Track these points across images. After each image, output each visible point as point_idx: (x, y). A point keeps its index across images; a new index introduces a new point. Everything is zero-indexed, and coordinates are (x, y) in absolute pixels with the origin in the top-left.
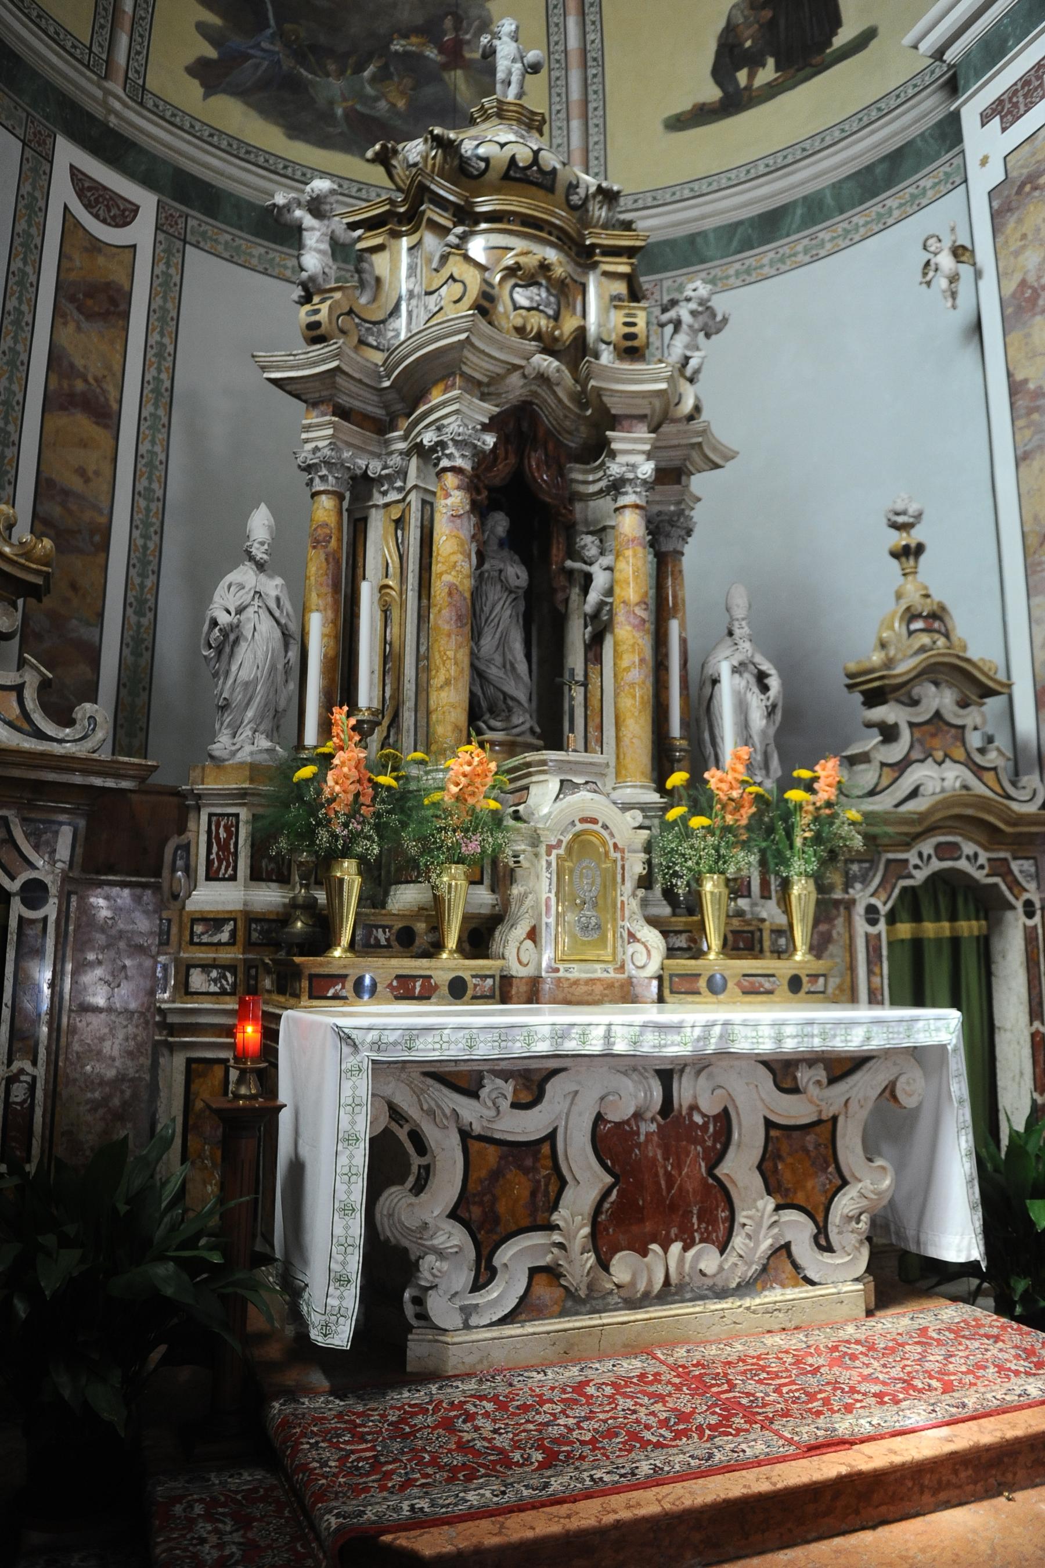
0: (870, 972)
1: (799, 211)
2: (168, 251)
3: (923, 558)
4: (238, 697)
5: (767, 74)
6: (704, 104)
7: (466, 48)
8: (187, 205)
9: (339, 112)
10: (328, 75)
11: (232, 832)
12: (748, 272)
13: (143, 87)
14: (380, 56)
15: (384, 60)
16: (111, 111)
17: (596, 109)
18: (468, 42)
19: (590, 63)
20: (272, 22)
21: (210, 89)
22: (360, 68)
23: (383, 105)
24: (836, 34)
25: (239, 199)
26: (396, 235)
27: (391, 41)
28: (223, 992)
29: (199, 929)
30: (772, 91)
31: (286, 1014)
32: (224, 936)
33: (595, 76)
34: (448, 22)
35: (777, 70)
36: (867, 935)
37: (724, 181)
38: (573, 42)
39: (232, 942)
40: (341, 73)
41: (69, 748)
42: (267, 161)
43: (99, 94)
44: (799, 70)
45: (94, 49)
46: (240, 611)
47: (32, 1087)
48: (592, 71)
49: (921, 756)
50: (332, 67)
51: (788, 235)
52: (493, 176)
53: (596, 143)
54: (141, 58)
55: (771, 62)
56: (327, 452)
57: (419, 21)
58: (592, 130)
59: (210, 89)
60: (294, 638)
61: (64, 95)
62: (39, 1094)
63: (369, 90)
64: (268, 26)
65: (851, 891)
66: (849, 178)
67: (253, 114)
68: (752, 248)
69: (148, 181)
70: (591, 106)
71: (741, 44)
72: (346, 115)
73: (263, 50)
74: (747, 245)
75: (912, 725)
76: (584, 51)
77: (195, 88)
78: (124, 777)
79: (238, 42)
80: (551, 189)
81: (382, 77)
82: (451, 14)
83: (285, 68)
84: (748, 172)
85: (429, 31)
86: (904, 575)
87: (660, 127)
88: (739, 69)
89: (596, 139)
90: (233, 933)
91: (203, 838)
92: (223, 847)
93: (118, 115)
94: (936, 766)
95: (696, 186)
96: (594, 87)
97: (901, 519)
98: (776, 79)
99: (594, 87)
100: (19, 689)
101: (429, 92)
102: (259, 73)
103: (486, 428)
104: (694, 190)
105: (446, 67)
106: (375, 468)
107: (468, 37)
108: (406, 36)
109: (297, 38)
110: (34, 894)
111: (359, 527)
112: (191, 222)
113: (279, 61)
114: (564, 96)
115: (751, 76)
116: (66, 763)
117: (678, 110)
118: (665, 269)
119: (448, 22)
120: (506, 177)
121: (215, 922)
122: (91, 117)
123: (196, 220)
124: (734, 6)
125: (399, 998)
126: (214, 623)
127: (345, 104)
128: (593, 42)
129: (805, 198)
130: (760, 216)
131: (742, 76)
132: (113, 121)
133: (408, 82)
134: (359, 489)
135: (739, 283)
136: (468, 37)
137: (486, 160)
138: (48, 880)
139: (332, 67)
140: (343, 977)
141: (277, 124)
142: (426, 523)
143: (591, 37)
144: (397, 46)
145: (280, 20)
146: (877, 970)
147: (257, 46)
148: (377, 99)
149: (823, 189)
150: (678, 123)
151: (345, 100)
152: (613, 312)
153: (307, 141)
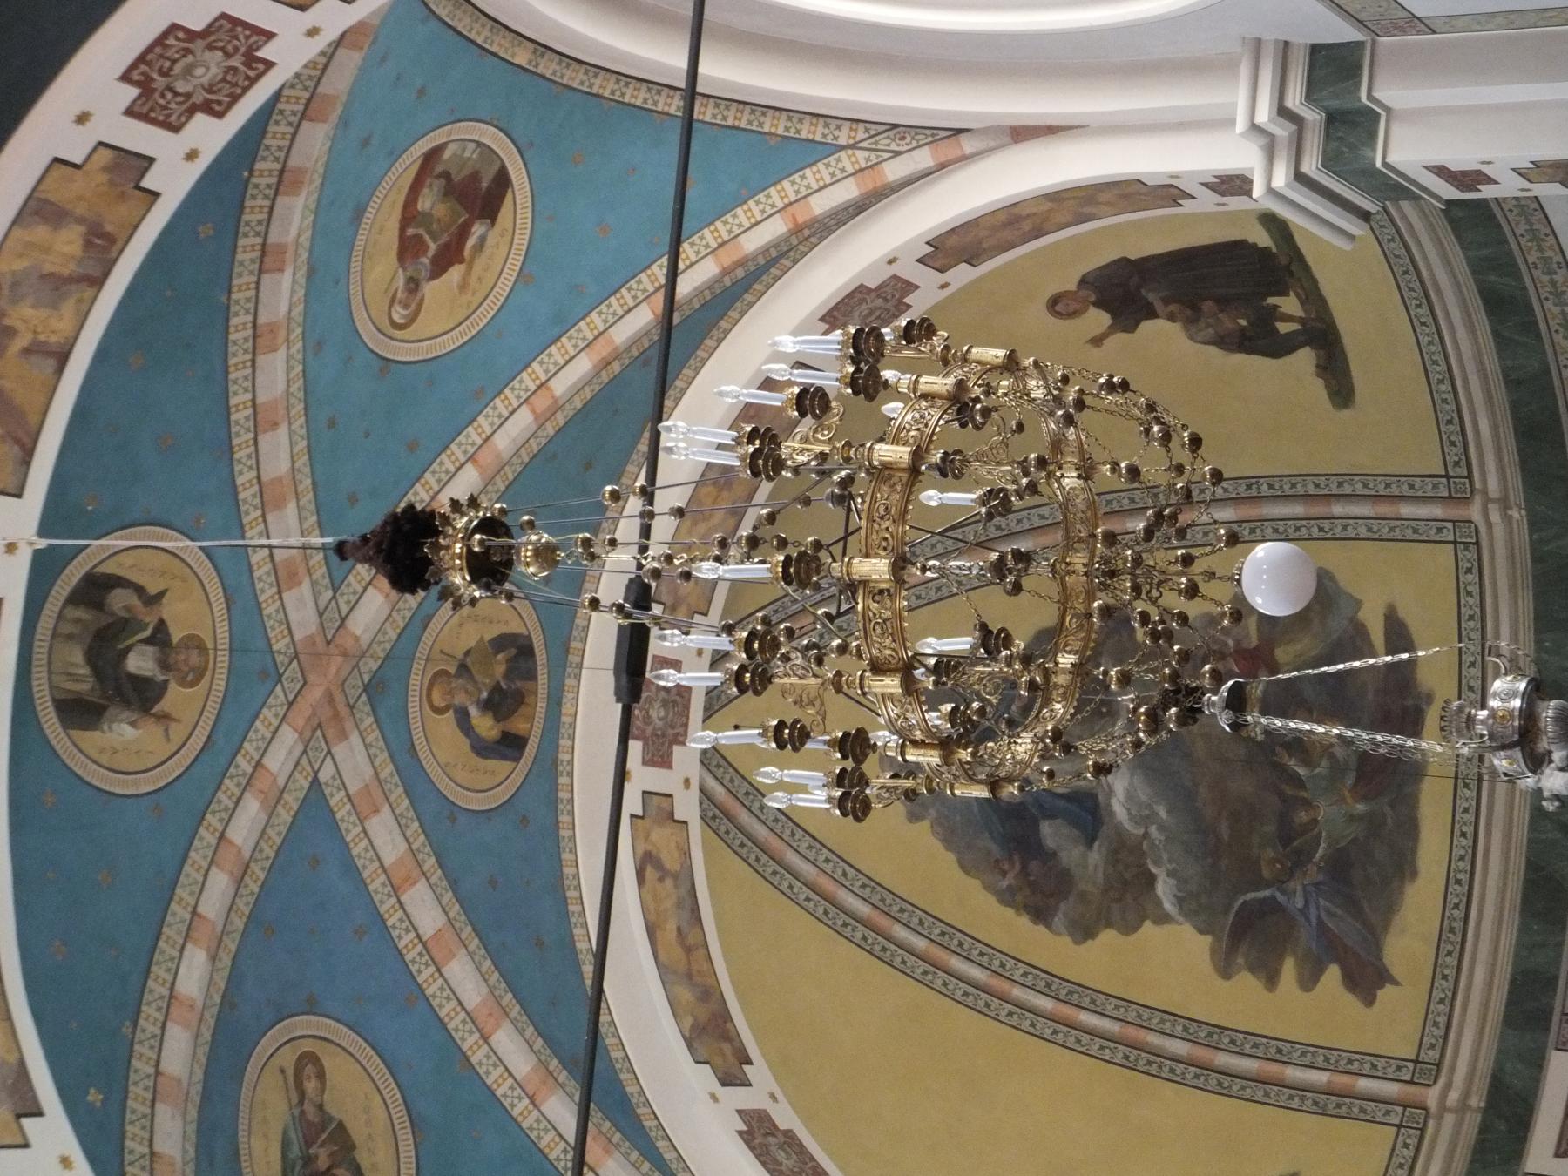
6: (1318, 366)
7: (1245, 645)
8: (1551, 1013)
9: (1361, 808)
10: (1315, 821)
13: (1416, 1062)
14: (1273, 752)
15: (1278, 749)
16: (1463, 1106)
17: (1317, 486)
18: (1238, 642)
19: (1254, 492)
20: (1267, 893)
21: (1383, 977)
24: (1255, 246)
25: (1520, 944)
27: (1253, 740)
30: (1313, 297)
33: (1271, 487)
35: (1284, 293)
37: (1433, 348)
42: (1456, 906)
43: (1449, 1119)
44: (1291, 274)
45: (1397, 1121)
50: (1302, 816)
51: (1525, 289)
53: (1365, 486)
54: (1380, 1063)
55: (1271, 300)
58: (1347, 489)
59: (1383, 977)
61: (1472, 1162)
64: (1273, 898)
67: (1397, 921)
68: (1536, 323)
69: (1537, 1064)
70: (1311, 490)
71: (1243, 329)
72: (1365, 798)
73: (1306, 902)
74: (1530, 326)
77: (1386, 994)
79: (1305, 935)
83: (1321, 877)
87: (1345, 414)
89: (1359, 486)
93: (1466, 1095)
96: (1287, 487)
98: (1298, 296)
99: (1287, 487)
102: (1339, 912)
107: (1231, 643)
109: (1278, 861)
113: (1316, 885)
114: (1299, 523)
115: (1288, 318)
117: (1324, 393)
122: (1484, 1129)
124: (1191, 338)
127: (1349, 800)
129: (1474, 273)
131: (1284, 328)
132: (1478, 1101)
136: (1231, 643)
139: (1302, 816)
141: (1402, 893)
145: (1259, 884)
147: (1304, 911)
149: (1467, 258)
150: (1341, 390)
151: (1343, 800)
152: (1247, 100)
153: (1414, 851)
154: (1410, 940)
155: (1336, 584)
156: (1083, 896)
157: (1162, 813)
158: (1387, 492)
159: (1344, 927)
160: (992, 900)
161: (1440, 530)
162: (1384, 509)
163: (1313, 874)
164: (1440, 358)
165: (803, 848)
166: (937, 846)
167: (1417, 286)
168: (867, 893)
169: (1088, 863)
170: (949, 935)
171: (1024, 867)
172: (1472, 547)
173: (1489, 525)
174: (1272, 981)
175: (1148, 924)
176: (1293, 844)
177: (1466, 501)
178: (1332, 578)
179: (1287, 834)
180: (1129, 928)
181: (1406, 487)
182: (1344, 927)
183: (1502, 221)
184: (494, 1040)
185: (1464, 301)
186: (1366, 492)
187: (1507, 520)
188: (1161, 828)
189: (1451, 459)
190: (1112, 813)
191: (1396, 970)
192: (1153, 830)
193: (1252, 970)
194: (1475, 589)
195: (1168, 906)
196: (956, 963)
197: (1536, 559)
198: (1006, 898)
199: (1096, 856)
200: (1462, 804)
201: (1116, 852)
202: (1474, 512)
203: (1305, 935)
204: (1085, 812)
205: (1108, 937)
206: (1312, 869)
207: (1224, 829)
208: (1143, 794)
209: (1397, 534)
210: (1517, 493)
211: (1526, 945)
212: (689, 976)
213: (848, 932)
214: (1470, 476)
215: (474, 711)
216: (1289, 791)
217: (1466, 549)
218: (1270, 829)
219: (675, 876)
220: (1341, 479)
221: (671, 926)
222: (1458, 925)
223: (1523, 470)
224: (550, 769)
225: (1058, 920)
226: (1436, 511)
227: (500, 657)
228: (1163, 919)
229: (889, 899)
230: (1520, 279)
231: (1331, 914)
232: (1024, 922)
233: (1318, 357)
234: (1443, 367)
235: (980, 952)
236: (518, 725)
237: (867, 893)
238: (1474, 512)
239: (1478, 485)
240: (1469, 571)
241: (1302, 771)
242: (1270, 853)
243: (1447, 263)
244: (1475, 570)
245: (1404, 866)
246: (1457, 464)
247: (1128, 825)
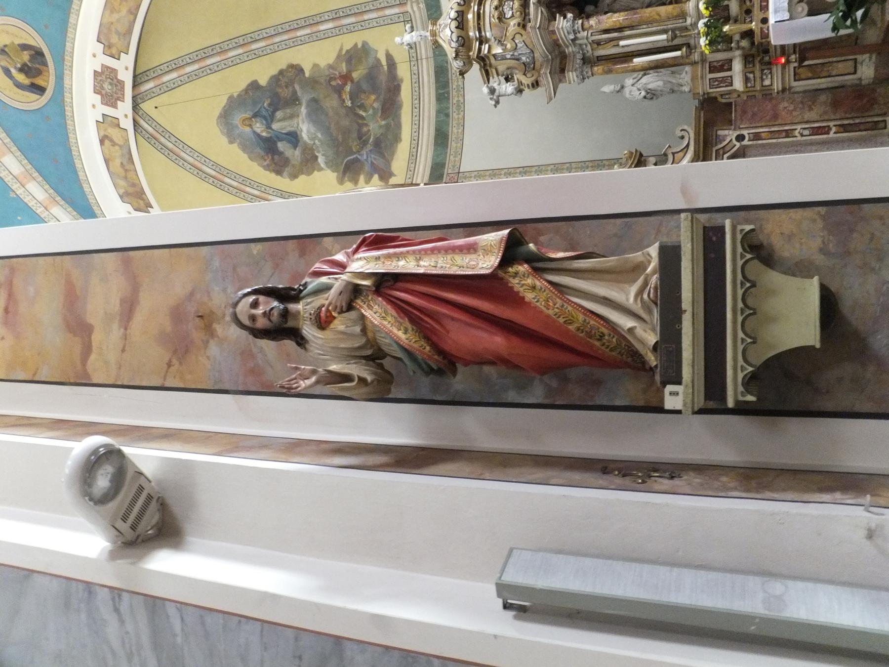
2: (465, 178)
4: (669, 86)
11: (716, 79)
22: (362, 118)
23: (376, 105)
26: (491, 66)
28: (771, 73)
29: (749, 85)
31: (773, 42)
32: (751, 76)
34: (333, 83)
38: (330, 25)
39: (753, 72)
40: (366, 125)
41: (692, 135)
46: (639, 90)
47: (805, 129)
52: (463, 34)
56: (578, 72)
57: (336, 96)
58: (367, 8)
59: (391, 174)
60: (646, 69)
62: (807, 126)
63: (371, 112)
67: (396, 157)
72: (384, 119)
78: (700, 116)
79: (367, 168)
80: (462, 12)
81: (362, 107)
82: (329, 82)
85: (339, 91)
90: (750, 73)
91: (718, 90)
92: (721, 82)
100: (673, 154)
101: (365, 86)
103: (565, 17)
105: (352, 81)
106: (579, 56)
108: (344, 101)
110: (740, 138)
111: (600, 59)
112: (450, 171)
116: (697, 134)
119: (333, 83)
120: (462, 29)
121: (747, 80)
123: (448, 170)
125: (768, 9)
126: (645, 97)
133: (363, 96)
134: (585, 60)
137: (458, 37)
138: (735, 135)
139: (365, 129)
140: (761, 29)
143: (327, 18)
144: (349, 103)
148: (374, 108)
154: (399, 163)
156: (293, 166)
157: (319, 135)
159: (379, 162)
160: (261, 169)
162: (381, 13)
163: (370, 147)
165: (188, 152)
166: (240, 152)
168: (214, 167)
169: (295, 155)
170: (245, 181)
171: (273, 159)
174: (356, 182)
175: (316, 172)
176: (362, 139)
178: (367, 44)
179: (360, 138)
180: (309, 173)
182: (379, 162)
184: (27, 187)
187: (419, 8)
188: (320, 140)
190: (302, 138)
191: (395, 172)
192: (316, 141)
193: (350, 181)
195: (322, 165)
196: (248, 189)
198: (267, 168)
199: (297, 152)
200: (414, 114)
201: (305, 150)
203: (367, 168)
204: (293, 138)
205: (302, 178)
206: (369, 146)
207: (340, 138)
208: (313, 129)
211: (436, 155)
212: (126, 178)
213: (207, 180)
215: (13, 71)
216: (360, 122)
218: (355, 135)
219: (120, 146)
221: (118, 162)
222: (414, 154)
224: (60, 102)
225: (285, 174)
227: (25, 52)
228: (320, 169)
229: (223, 169)
231: (375, 159)
232: (273, 175)
235: (251, 183)
236: (40, 81)
237: (214, 167)
241: (364, 114)
242: (355, 143)
245: (397, 139)
247: (309, 141)
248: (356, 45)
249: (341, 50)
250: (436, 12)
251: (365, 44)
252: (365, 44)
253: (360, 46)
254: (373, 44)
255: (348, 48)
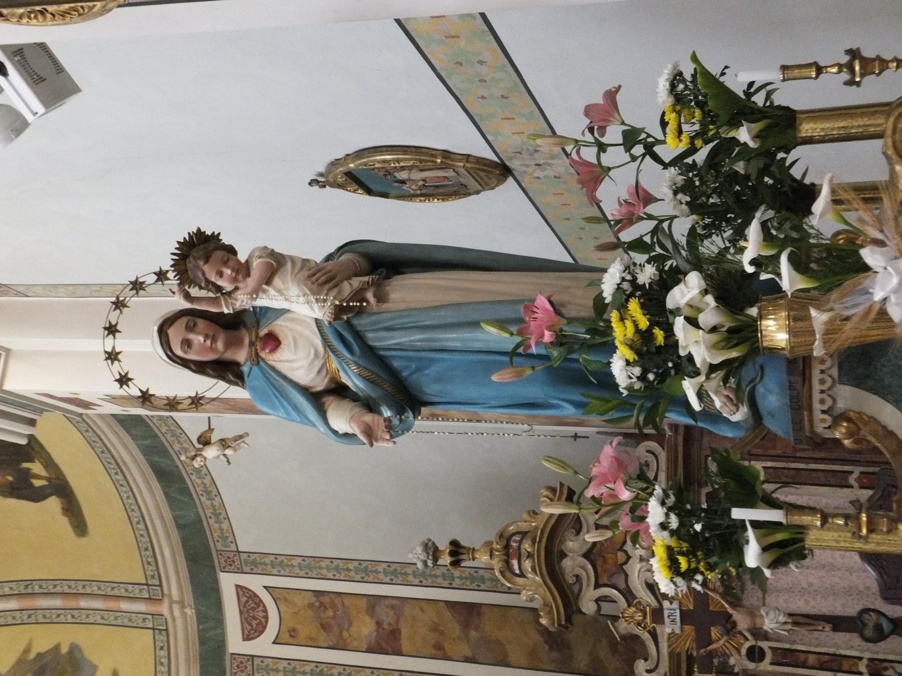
0: (804, 666)
1: (156, 459)
3: (463, 543)
5: (36, 467)
6: (63, 508)
12: (209, 493)
17: (70, 587)
19: (29, 590)
30: (49, 463)
33: (41, 587)
36: (772, 664)
37: (130, 501)
44: (33, 449)
48: (37, 590)
49: (623, 577)
51: (177, 467)
53: (99, 588)
55: (25, 465)
58: (88, 590)
65: (736, 670)
66: (127, 432)
70: (67, 590)
71: (11, 483)
74: (185, 491)
75: (597, 586)
76: (20, 595)
84: (122, 485)
86: (474, 560)
87: (84, 540)
88: (31, 485)
89: (96, 588)
94: (631, 561)
95: (135, 520)
97: (430, 563)
98: (41, 463)
104: (138, 522)
115: (38, 477)
118: (207, 546)
128: (11, 589)
129: (144, 455)
130: (160, 481)
131: (37, 483)
135: (218, 498)
141: (879, 585)
142: (452, 156)
146: (802, 657)
149: (138, 446)
150: (80, 526)
155: (83, 656)
158: (112, 593)
161: (144, 620)
164: (135, 508)
167: (112, 460)
172: (164, 632)
173: (174, 619)
177: (159, 601)
178: (80, 650)
181: (123, 591)
183: (152, 425)
185: (143, 473)
186: (100, 592)
187: (184, 615)
189: (149, 573)
194: (165, 661)
197: (202, 642)
202: (164, 609)
209: (119, 622)
210: (189, 598)
214: (160, 585)
217: (160, 634)
220: (84, 583)
223: (192, 582)
226: (141, 607)
230: (173, 461)
233: (62, 503)
234: (138, 514)
238: (164, 609)
239: (166, 591)
240: (162, 648)
243: (126, 448)
244: (165, 648)
246: (153, 577)
248: (57, 647)
249: (27, 651)
250: (215, 628)
251: (74, 650)
252: (74, 650)
253: (64, 650)
254: (90, 653)
255: (42, 650)
